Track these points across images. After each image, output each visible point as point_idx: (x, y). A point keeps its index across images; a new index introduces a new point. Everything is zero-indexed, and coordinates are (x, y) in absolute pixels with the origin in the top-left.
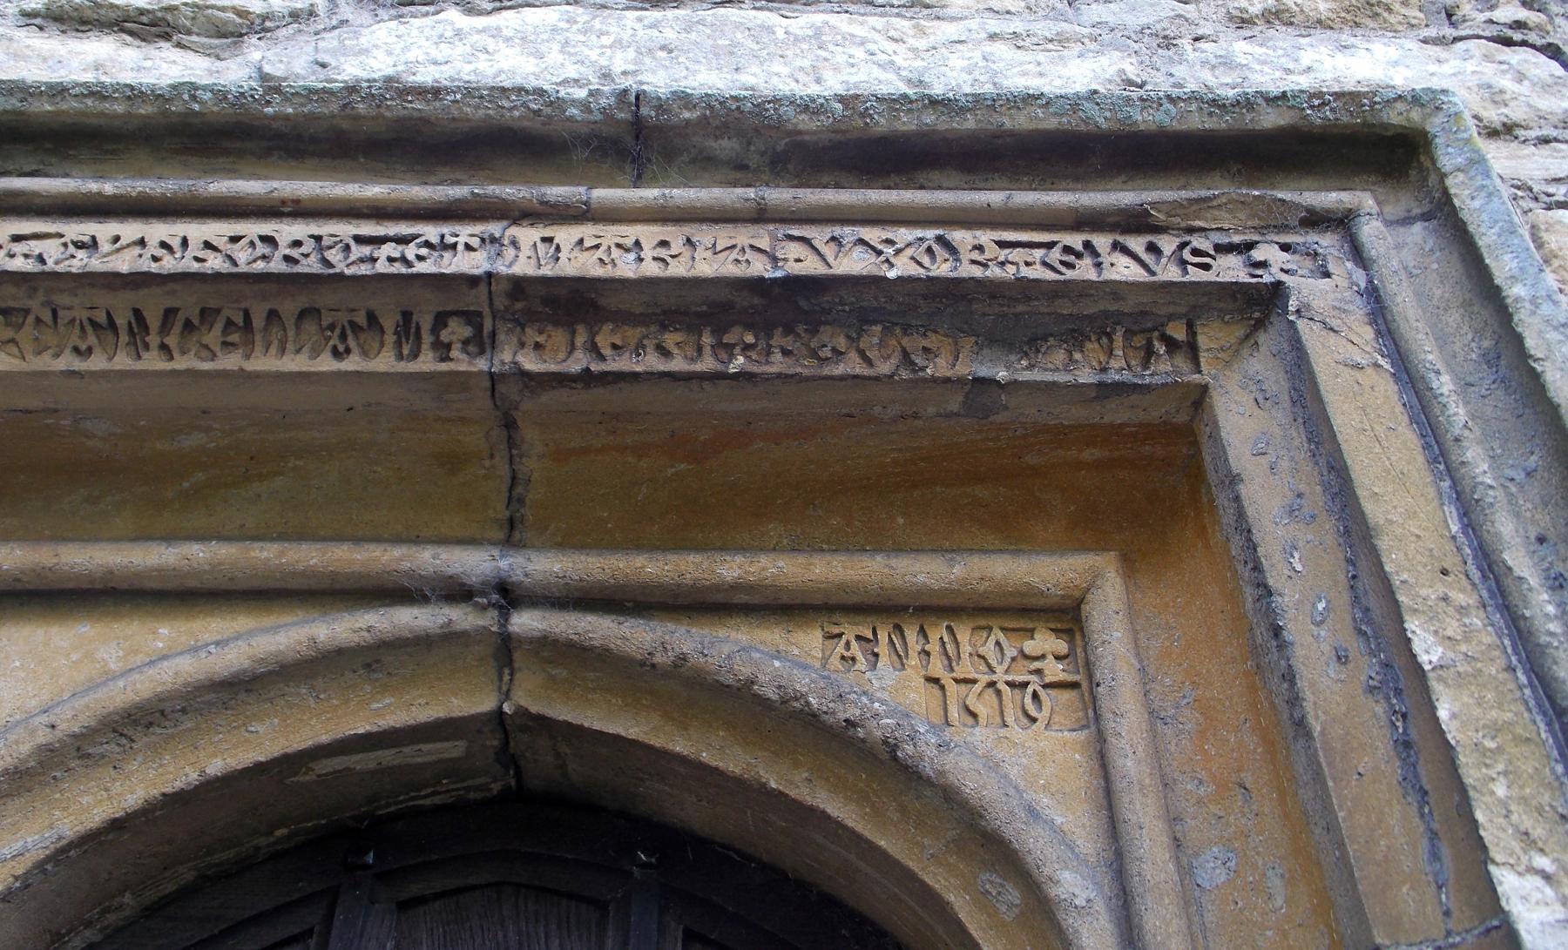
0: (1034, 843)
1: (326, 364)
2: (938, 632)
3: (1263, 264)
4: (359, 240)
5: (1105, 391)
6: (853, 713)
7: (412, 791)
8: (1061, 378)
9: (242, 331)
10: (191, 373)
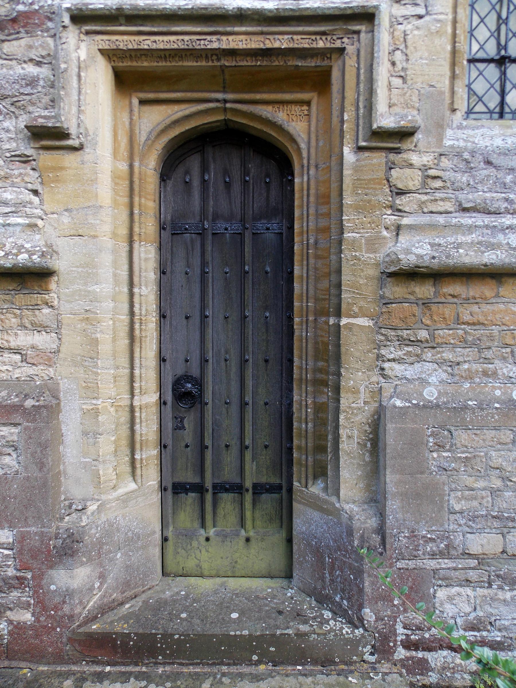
0: (299, 140)
1: (195, 64)
2: (289, 106)
3: (343, 43)
4: (198, 40)
5: (316, 67)
6: (275, 120)
7: (497, 403)
8: (309, 65)
9: (181, 58)
10: (175, 66)
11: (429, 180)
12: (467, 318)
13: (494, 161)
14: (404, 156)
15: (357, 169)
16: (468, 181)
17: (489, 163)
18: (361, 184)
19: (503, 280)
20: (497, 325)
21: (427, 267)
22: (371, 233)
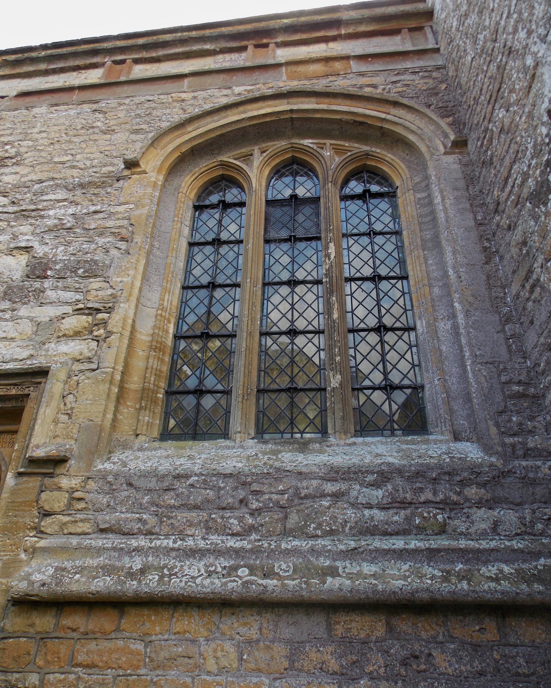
11: (74, 501)
12: (80, 658)
13: (134, 483)
14: (56, 480)
15: (14, 492)
16: (108, 502)
17: (130, 485)
18: (14, 506)
19: (126, 609)
20: (113, 668)
21: (37, 595)
22: (10, 555)
